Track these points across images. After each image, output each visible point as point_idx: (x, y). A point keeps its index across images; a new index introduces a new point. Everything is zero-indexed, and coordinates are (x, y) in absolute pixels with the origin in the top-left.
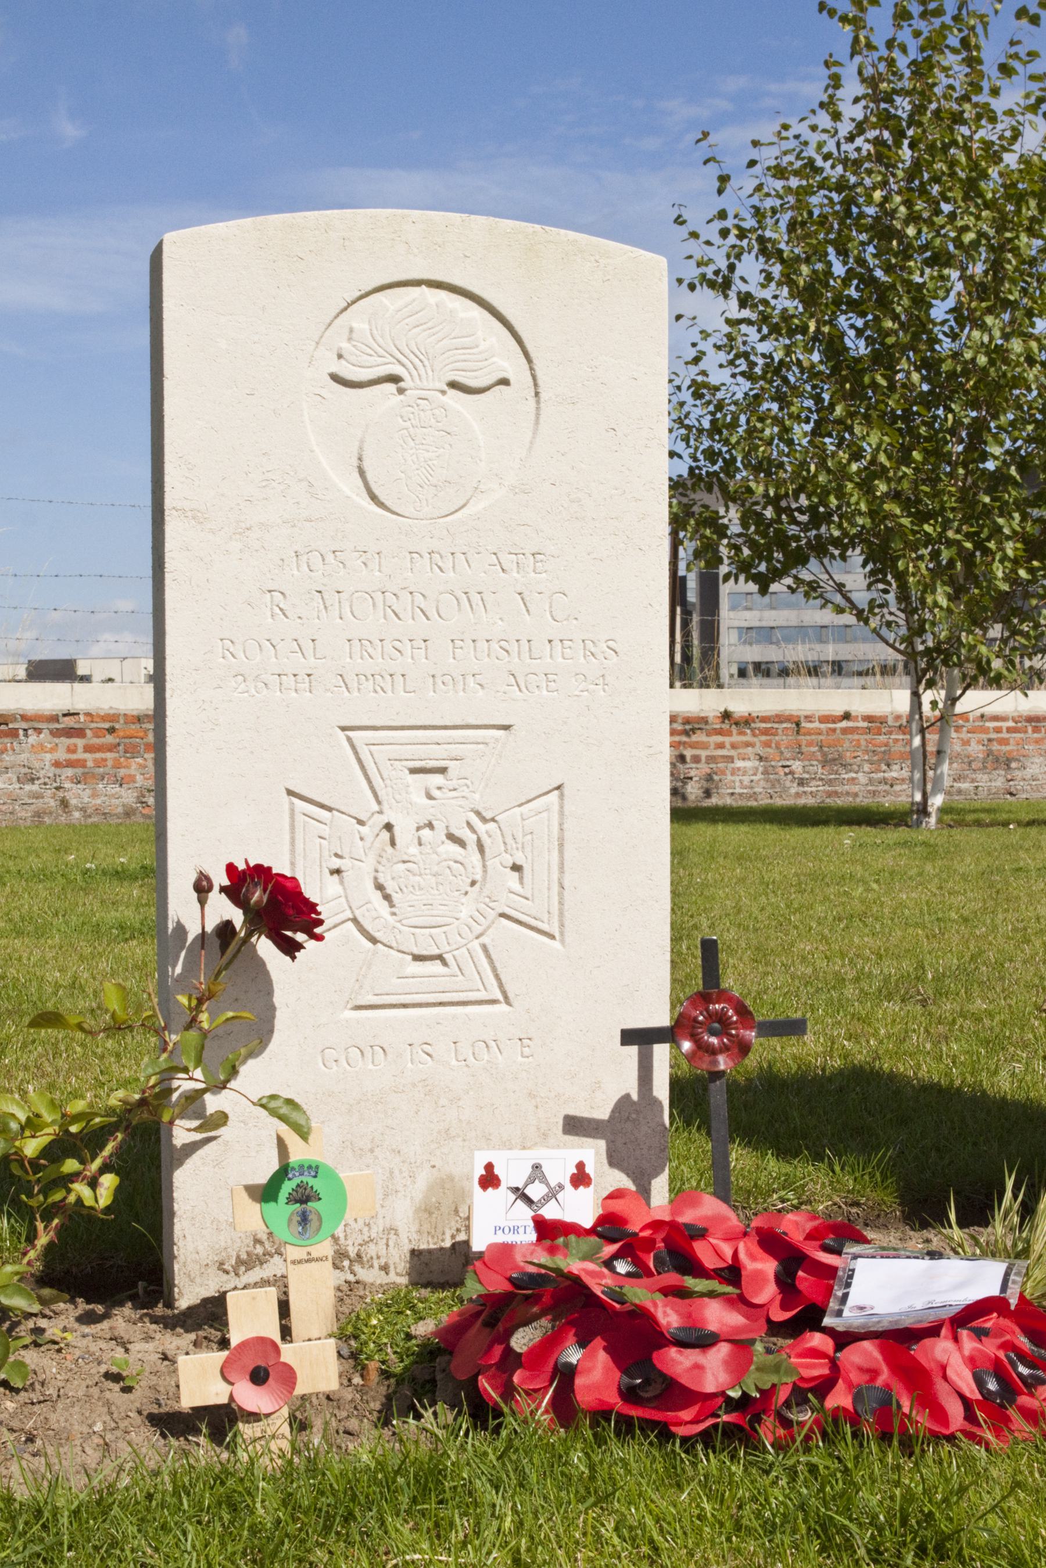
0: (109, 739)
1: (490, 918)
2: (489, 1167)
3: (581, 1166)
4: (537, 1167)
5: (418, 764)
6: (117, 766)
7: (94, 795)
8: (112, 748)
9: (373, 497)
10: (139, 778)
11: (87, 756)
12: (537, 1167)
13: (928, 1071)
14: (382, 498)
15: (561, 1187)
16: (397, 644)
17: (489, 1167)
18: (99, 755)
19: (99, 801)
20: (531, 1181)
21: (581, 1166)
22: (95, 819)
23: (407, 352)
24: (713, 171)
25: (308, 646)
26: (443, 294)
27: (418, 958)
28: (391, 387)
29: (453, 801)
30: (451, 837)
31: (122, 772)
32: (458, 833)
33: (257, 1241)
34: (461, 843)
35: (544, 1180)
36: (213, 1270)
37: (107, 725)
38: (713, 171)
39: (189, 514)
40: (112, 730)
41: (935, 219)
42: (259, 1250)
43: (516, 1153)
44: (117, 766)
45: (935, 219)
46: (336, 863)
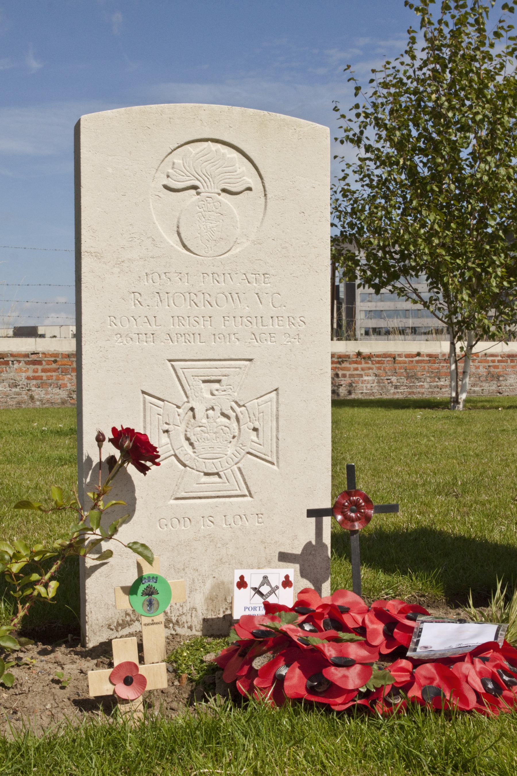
0: (54, 366)
1: (242, 454)
2: (242, 578)
3: (287, 577)
4: (265, 578)
5: (206, 378)
6: (58, 379)
7: (47, 393)
8: (55, 370)
9: (185, 246)
10: (69, 385)
11: (43, 374)
12: (265, 578)
13: (459, 530)
14: (189, 246)
15: (277, 587)
16: (196, 319)
17: (242, 578)
18: (49, 374)
19: (49, 397)
20: (262, 584)
21: (287, 577)
22: (47, 405)
23: (201, 174)
24: (352, 85)
25: (152, 320)
26: (219, 146)
27: (207, 474)
28: (193, 192)
29: (224, 397)
30: (223, 414)
31: (60, 382)
32: (226, 412)
33: (127, 614)
34: (228, 417)
35: (269, 584)
36: (105, 629)
37: (53, 359)
38: (352, 85)
39: (94, 254)
40: (55, 362)
41: (462, 108)
42: (128, 619)
43: (255, 571)
44: (58, 379)
45: (462, 108)
46: (166, 427)
